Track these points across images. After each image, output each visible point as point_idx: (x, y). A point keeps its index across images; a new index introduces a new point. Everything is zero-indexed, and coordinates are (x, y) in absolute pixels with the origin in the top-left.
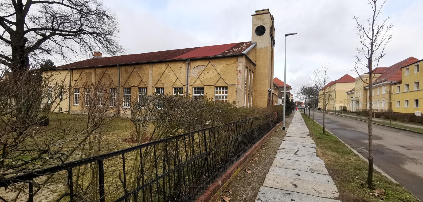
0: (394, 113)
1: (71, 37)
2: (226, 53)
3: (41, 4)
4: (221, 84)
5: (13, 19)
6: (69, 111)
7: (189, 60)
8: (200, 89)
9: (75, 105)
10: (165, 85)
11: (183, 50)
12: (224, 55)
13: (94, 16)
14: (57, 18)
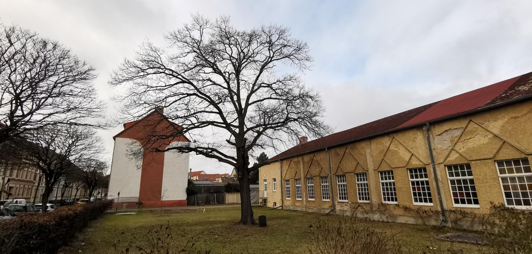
0: (330, 152)
1: (279, 128)
2: (502, 99)
3: (255, 104)
4: (507, 154)
5: (236, 123)
6: (282, 206)
7: (428, 124)
8: (389, 174)
9: (323, 200)
10: (393, 166)
11: (410, 112)
12: (499, 103)
13: (298, 101)
14: (267, 112)
